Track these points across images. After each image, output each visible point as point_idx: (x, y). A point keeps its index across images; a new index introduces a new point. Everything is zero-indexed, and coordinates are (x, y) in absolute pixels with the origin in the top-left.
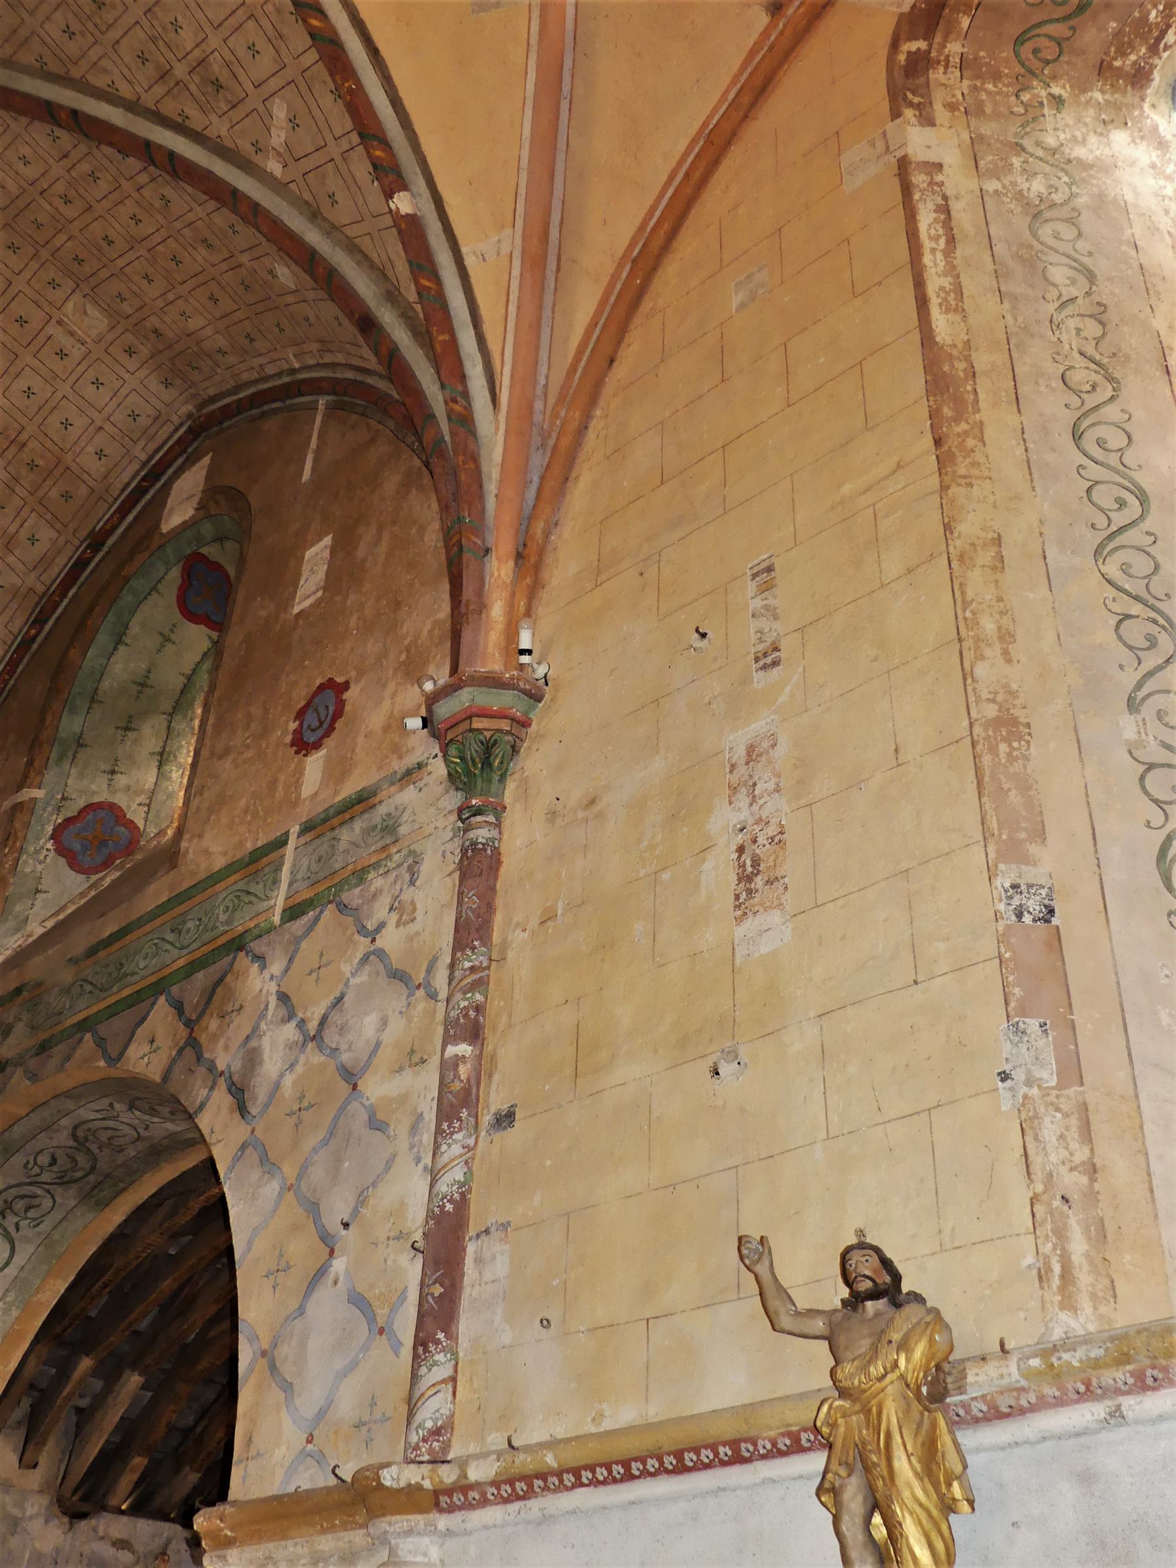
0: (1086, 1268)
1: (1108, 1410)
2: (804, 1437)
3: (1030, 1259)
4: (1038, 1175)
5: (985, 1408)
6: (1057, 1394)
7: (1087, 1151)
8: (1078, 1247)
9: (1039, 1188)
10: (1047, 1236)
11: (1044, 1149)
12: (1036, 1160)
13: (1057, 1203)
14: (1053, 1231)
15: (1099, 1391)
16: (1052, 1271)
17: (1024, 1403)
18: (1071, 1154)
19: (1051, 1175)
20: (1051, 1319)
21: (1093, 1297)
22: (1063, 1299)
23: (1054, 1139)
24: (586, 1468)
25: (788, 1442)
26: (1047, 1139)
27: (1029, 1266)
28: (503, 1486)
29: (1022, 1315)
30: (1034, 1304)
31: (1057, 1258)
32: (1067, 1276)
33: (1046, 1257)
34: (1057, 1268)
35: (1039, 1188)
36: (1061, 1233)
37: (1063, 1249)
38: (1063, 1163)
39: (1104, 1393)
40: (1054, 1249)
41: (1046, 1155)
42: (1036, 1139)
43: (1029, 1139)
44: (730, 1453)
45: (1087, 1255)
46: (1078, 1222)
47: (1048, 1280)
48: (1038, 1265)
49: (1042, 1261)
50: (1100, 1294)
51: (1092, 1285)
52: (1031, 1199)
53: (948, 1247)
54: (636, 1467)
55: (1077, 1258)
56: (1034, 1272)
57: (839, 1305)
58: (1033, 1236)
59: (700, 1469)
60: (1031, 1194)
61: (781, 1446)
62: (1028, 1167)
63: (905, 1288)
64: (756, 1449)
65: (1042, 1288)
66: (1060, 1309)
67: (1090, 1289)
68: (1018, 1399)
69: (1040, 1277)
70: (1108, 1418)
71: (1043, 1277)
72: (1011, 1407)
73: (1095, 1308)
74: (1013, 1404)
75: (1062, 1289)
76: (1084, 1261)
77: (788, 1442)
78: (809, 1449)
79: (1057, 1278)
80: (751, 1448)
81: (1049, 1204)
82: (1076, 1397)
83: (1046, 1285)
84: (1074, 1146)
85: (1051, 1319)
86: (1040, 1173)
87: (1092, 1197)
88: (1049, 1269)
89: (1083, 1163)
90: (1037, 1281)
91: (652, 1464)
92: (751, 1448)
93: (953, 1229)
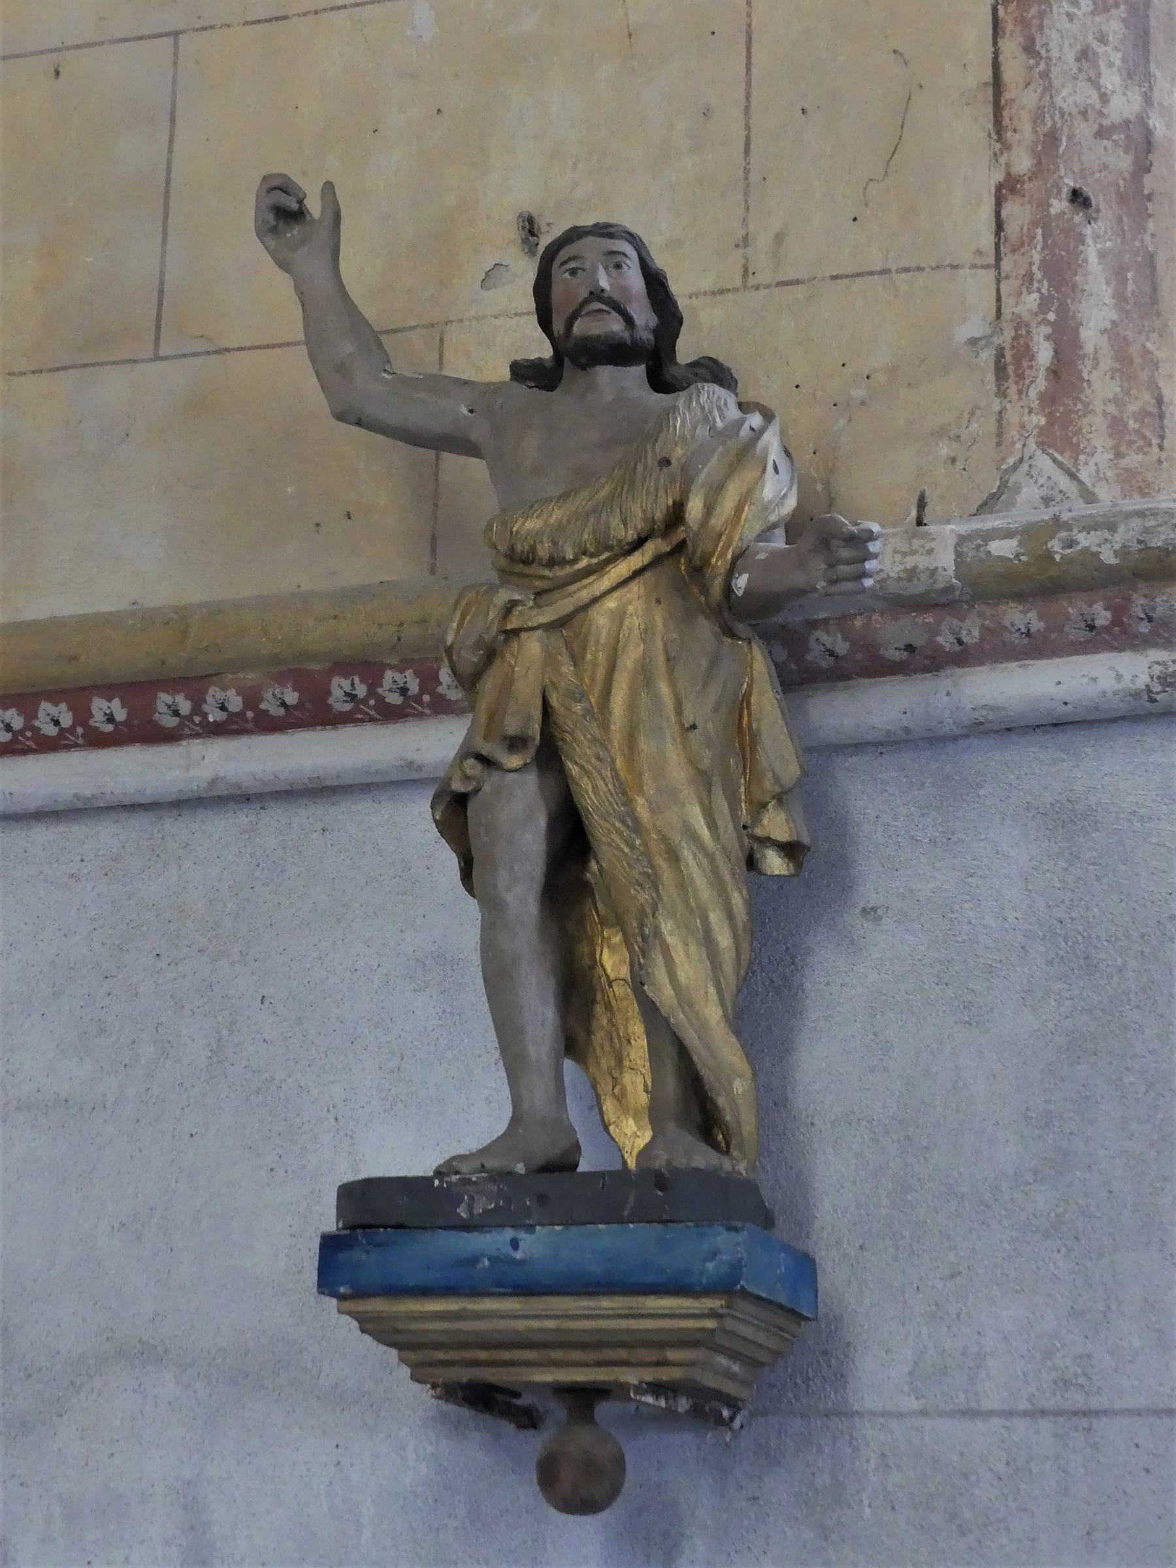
0: (1106, 363)
1: (1157, 670)
2: (339, 686)
3: (975, 327)
4: (1024, 133)
5: (842, 648)
6: (1037, 626)
7: (1136, 98)
8: (1096, 315)
9: (1023, 163)
10: (1029, 278)
11: (1045, 75)
12: (1024, 100)
13: (1059, 205)
14: (1044, 266)
15: (1144, 628)
16: (1032, 358)
17: (945, 641)
18: (1104, 98)
19: (1052, 138)
20: (1015, 468)
21: (1117, 426)
22: (1051, 423)
23: (1070, 56)
24: (344, 667)
25: (292, 698)
26: (1055, 54)
27: (973, 342)
28: (46, 707)
29: (945, 450)
30: (983, 426)
31: (1046, 330)
32: (1065, 371)
33: (1020, 324)
34: (1044, 355)
35: (1023, 163)
36: (1061, 274)
37: (1063, 311)
38: (1084, 113)
39: (1154, 633)
40: (1044, 306)
41: (1048, 89)
42: (1029, 48)
43: (1010, 47)
44: (121, 715)
45: (1112, 332)
46: (1102, 255)
47: (1021, 376)
48: (996, 340)
49: (1008, 334)
50: (1132, 424)
51: (1115, 400)
52: (999, 187)
53: (764, 277)
54: (169, 705)
55: (1091, 336)
56: (987, 356)
57: (505, 374)
58: (992, 273)
59: (25, 752)
60: (999, 176)
61: (270, 706)
62: (998, 109)
63: (686, 349)
64: (197, 708)
65: (1002, 394)
66: (1041, 445)
67: (1111, 409)
68: (933, 631)
69: (1000, 370)
70: (1156, 688)
71: (1008, 367)
72: (910, 648)
73: (1118, 455)
74: (919, 641)
75: (1049, 400)
76: (1104, 342)
77: (292, 698)
78: (347, 719)
79: (1042, 373)
80: (185, 707)
81: (1044, 205)
82: (1083, 635)
83: (1013, 390)
84: (1111, 80)
85: (1015, 468)
86: (1027, 128)
87: (1137, 199)
88: (1025, 353)
89: (1126, 124)
90: (991, 377)
91: (106, 710)
92: (185, 707)
93: (779, 238)
